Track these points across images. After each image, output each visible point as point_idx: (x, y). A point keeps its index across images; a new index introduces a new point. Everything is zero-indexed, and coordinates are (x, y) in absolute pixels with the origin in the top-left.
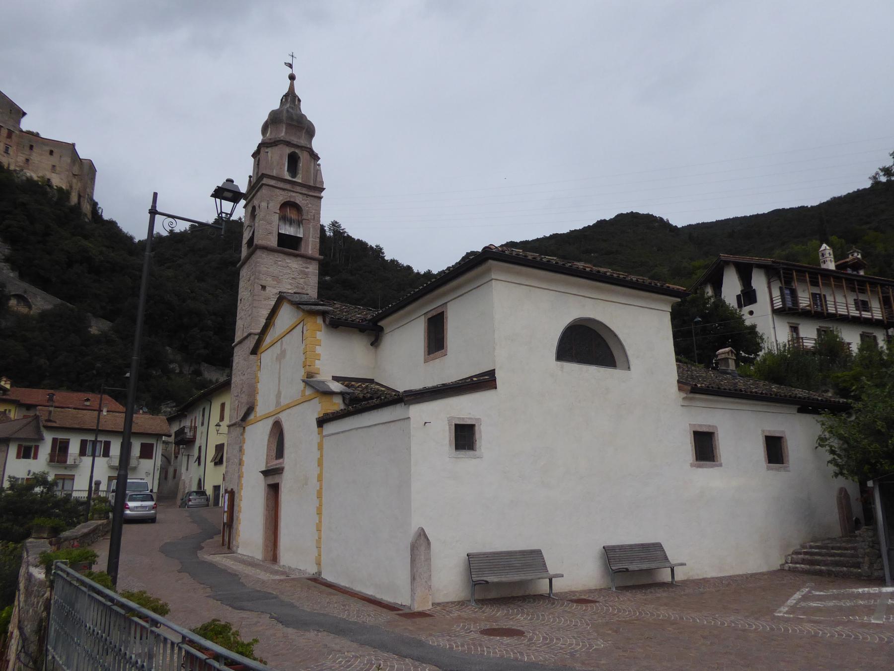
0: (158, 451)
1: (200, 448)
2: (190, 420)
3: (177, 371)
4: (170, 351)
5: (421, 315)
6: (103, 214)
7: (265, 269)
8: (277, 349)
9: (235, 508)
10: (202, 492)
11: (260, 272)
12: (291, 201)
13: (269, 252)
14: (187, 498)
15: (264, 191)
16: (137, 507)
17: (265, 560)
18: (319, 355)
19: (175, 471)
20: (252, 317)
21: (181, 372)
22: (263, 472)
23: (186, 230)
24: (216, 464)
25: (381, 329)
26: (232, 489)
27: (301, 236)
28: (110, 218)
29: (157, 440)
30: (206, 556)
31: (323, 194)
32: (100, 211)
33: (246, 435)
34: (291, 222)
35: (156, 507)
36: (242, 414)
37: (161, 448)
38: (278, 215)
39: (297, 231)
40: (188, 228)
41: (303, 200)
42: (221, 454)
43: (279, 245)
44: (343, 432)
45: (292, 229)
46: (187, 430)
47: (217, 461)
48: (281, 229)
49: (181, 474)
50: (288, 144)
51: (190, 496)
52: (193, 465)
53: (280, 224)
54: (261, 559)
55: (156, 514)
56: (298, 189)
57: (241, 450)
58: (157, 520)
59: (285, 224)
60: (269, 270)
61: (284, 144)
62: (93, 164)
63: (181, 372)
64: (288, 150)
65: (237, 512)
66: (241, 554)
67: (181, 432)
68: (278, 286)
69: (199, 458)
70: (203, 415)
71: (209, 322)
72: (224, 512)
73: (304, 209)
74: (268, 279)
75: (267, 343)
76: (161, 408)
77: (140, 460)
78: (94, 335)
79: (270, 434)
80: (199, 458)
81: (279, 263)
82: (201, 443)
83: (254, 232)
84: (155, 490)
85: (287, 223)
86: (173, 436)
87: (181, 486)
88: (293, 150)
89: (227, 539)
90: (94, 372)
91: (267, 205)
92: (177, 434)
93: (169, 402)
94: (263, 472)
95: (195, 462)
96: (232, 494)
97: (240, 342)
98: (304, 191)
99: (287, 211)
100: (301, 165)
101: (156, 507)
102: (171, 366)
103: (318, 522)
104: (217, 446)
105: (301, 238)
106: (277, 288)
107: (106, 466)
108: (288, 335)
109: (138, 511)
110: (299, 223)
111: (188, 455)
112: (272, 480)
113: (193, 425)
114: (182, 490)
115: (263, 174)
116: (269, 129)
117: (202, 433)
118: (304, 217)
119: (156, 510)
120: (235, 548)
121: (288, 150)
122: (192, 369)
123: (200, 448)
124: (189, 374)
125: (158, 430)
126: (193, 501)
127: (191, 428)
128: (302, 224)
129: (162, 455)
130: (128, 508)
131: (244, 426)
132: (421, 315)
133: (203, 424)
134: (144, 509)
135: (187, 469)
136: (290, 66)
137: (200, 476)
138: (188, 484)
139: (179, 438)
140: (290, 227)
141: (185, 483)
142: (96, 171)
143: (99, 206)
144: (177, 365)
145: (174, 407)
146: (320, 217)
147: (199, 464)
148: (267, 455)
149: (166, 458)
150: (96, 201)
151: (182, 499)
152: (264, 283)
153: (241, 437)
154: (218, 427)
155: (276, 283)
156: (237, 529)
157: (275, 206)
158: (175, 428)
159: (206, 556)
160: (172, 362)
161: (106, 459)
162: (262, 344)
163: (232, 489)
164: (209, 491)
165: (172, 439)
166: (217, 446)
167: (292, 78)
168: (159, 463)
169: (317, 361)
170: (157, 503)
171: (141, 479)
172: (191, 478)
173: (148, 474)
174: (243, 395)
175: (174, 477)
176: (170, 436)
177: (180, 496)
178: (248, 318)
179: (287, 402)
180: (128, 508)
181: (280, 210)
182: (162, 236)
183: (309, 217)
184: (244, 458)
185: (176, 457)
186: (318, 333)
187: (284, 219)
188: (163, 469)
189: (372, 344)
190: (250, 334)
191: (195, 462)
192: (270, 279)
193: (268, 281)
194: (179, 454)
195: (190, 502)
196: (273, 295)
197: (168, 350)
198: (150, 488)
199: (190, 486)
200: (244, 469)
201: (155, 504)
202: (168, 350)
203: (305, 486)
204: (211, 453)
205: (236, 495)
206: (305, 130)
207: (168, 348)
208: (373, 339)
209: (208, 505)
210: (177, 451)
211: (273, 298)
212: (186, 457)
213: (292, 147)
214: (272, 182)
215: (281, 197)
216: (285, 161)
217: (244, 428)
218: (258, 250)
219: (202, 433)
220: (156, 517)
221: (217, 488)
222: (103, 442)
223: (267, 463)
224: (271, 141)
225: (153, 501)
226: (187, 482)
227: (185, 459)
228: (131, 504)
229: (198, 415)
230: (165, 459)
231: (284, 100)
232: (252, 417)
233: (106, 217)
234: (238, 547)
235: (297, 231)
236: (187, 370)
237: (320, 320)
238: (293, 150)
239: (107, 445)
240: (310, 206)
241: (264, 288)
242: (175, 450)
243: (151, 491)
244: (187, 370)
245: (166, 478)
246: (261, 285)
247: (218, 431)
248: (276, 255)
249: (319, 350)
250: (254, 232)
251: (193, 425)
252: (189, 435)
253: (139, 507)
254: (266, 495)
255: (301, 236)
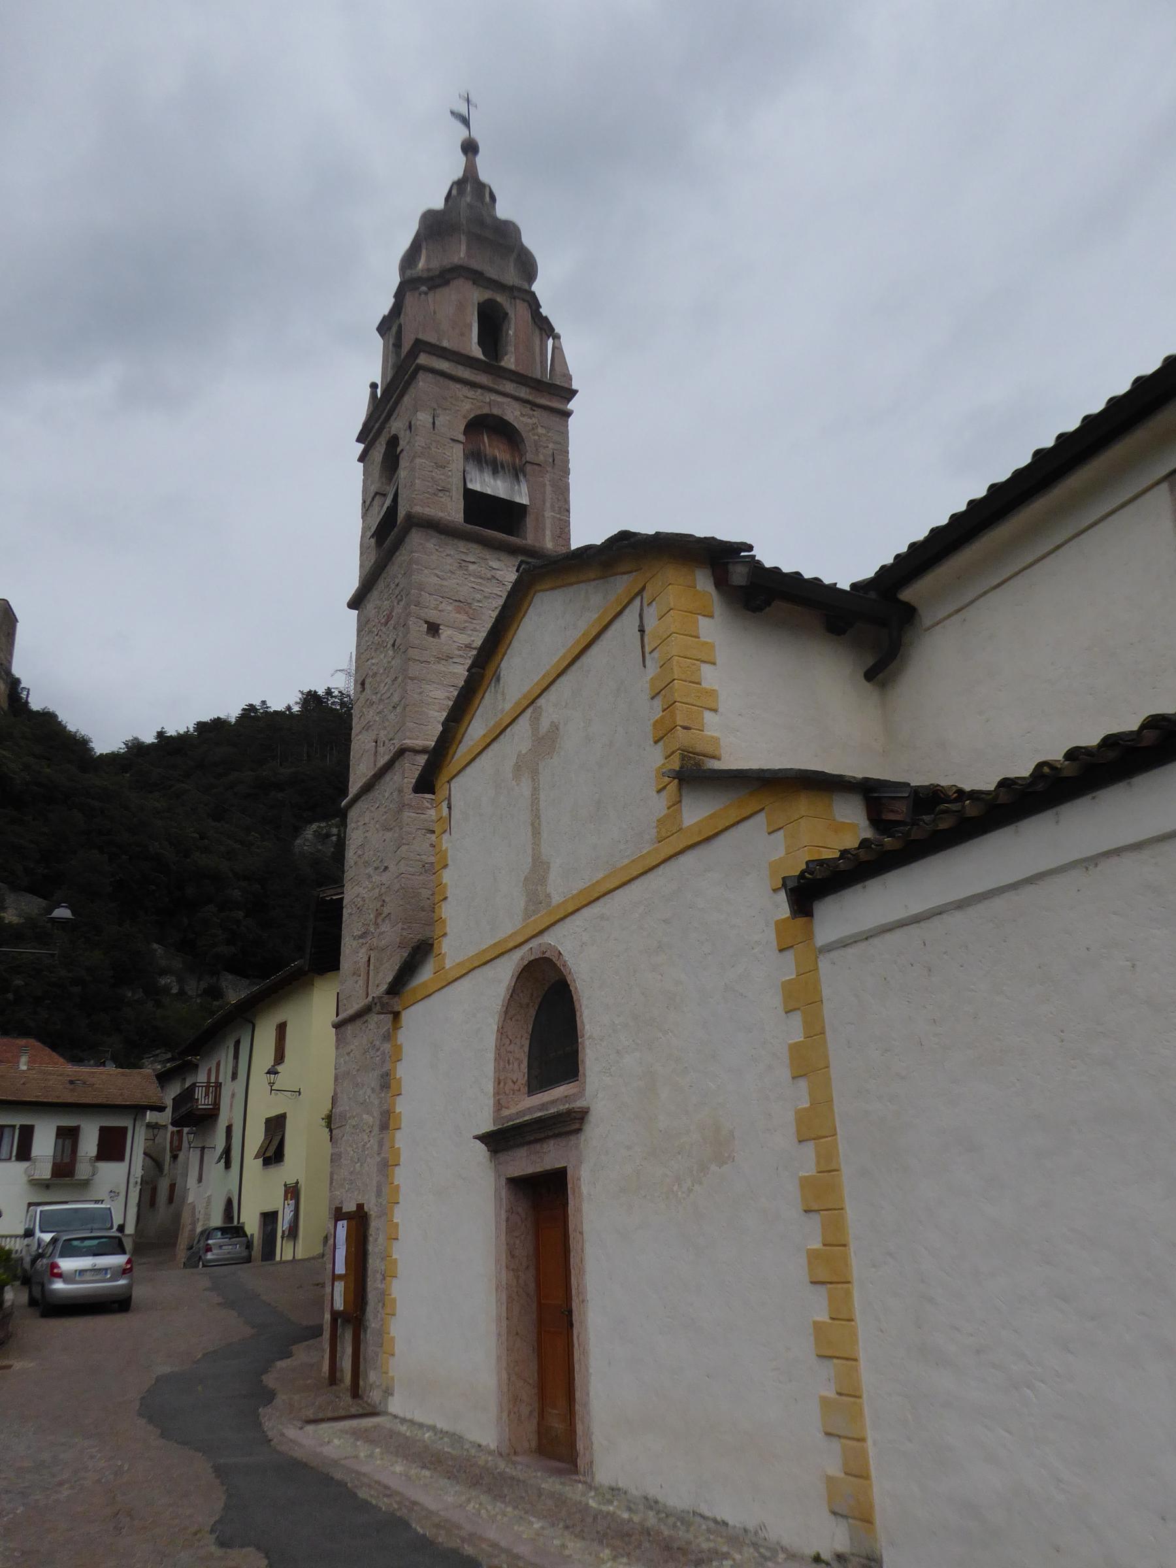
0: (137, 1144)
1: (229, 1129)
2: (206, 1072)
3: (175, 991)
4: (159, 950)
5: (1158, 483)
6: (30, 700)
7: (435, 580)
8: (520, 738)
9: (373, 1263)
10: (236, 1227)
11: (421, 587)
12: (493, 415)
13: (443, 537)
14: (202, 1244)
15: (424, 383)
16: (82, 1272)
17: (510, 1453)
18: (712, 693)
19: (172, 1187)
20: (405, 708)
21: (182, 992)
22: (485, 1138)
23: (188, 731)
24: (267, 1162)
25: (909, 613)
26: (360, 1207)
27: (524, 503)
28: (43, 707)
29: (135, 1120)
30: (292, 1432)
31: (571, 406)
32: (24, 695)
33: (403, 1036)
34: (496, 468)
35: (131, 1269)
36: (387, 976)
37: (143, 1138)
38: (461, 446)
39: (512, 489)
40: (191, 730)
41: (522, 415)
42: (280, 1137)
43: (467, 519)
44: (961, 905)
45: (499, 483)
46: (199, 1093)
47: (268, 1155)
48: (471, 480)
49: (186, 1190)
50: (477, 278)
51: (207, 1239)
52: (214, 1169)
53: (467, 468)
54: (493, 1446)
55: (129, 1287)
56: (509, 387)
57: (387, 1083)
58: (132, 1304)
59: (481, 470)
60: (445, 583)
61: (467, 278)
62: (9, 606)
63: (182, 992)
64: (476, 295)
65: (379, 1276)
66: (403, 1420)
67: (187, 1096)
68: (472, 626)
69: (227, 1152)
70: (236, 1057)
71: (237, 893)
72: (335, 1278)
73: (529, 438)
74: (441, 607)
75: (471, 743)
76: (144, 1063)
77: (97, 1164)
78: (10, 925)
79: (506, 1012)
80: (227, 1152)
81: (472, 567)
82: (230, 1119)
83: (396, 495)
84: (130, 1229)
85: (486, 470)
86: (169, 1111)
87: (186, 1218)
88: (487, 295)
89: (346, 1364)
90: (10, 996)
91: (431, 420)
92: (178, 1102)
93: (158, 1051)
94: (485, 1138)
95: (219, 1161)
96: (359, 1221)
97: (368, 788)
98: (523, 393)
99: (484, 442)
100: (511, 332)
101: (131, 1269)
102: (163, 981)
103: (823, 1317)
104: (268, 1121)
105: (523, 508)
106: (470, 632)
107: (24, 1179)
108: (563, 679)
109: (87, 1282)
110: (517, 472)
111: (203, 1148)
112: (524, 1163)
113: (213, 1080)
114: (189, 1227)
115: (418, 342)
116: (424, 252)
117: (233, 1095)
118: (529, 456)
119: (131, 1278)
120: (375, 1396)
121: (476, 295)
122: (203, 985)
123: (229, 1129)
124: (198, 996)
125: (138, 1098)
126: (215, 1251)
127: (207, 1087)
128: (525, 476)
129: (145, 1153)
130: (60, 1275)
131: (396, 1009)
132: (1158, 483)
133: (234, 1076)
134: (97, 1277)
135: (200, 1180)
136: (465, 121)
137: (230, 1191)
138: (202, 1211)
139: (183, 1110)
140: (495, 479)
141: (194, 1208)
142: (17, 621)
143: (22, 686)
144: (174, 978)
145: (168, 1060)
146: (568, 461)
147: (228, 1165)
148: (498, 1082)
149: (154, 1160)
150: (17, 676)
151: (191, 1248)
152: (433, 616)
153: (387, 1047)
154: (272, 1076)
155: (465, 617)
156: (382, 1332)
157: (453, 424)
158: (174, 1090)
159: (292, 1432)
160: (163, 972)
161: (25, 1165)
162: (451, 751)
163: (360, 1207)
164: (251, 1224)
165: (165, 1117)
166: (268, 1121)
167: (470, 148)
168: (138, 1172)
169: (708, 715)
170: (133, 1259)
171: (97, 1202)
172: (209, 1197)
173: (113, 1194)
174: (385, 927)
175: (171, 1200)
176: (161, 1109)
177: (183, 1243)
178: (392, 717)
179: (578, 885)
180: (60, 1275)
181: (465, 432)
182: (143, 743)
183: (541, 457)
184: (402, 1106)
185: (175, 1157)
186: (703, 622)
187: (476, 457)
188: (147, 1183)
189: (870, 676)
190: (401, 752)
191: (219, 1161)
192: (450, 608)
193: (446, 613)
194: (180, 1150)
195: (209, 1253)
196: (459, 649)
197: (156, 950)
198: (118, 1220)
199: (208, 1216)
200: (401, 1140)
201: (129, 1262)
202: (156, 950)
203: (714, 1168)
204: (256, 1137)
205: (374, 1224)
206: (514, 255)
207: (155, 946)
208: (870, 662)
209: (248, 1260)
210: (176, 1143)
211: (461, 656)
212: (198, 1152)
213: (487, 288)
214: (444, 365)
215: (469, 404)
216: (473, 314)
217: (396, 1016)
218: (414, 530)
219: (233, 1095)
220: (130, 1297)
221: (269, 1218)
222: (18, 1127)
223: (499, 1106)
224: (431, 274)
225: (124, 1252)
226: (200, 1208)
227: (194, 1156)
228: (67, 1264)
229: (225, 1057)
230: (153, 1163)
231: (454, 192)
232: (426, 974)
233: (36, 704)
234: (388, 1392)
235: (512, 489)
236: (193, 987)
237: (704, 582)
238: (487, 295)
239: (27, 1134)
240: (540, 430)
241: (433, 629)
242: (171, 1143)
243: (121, 1228)
244: (193, 987)
245: (153, 1203)
246: (426, 622)
247: (271, 1084)
248: (462, 545)
249: (709, 677)
250: (396, 495)
251: (213, 1080)
252: (203, 1100)
253: (86, 1271)
254: (504, 1216)
255: (524, 500)
